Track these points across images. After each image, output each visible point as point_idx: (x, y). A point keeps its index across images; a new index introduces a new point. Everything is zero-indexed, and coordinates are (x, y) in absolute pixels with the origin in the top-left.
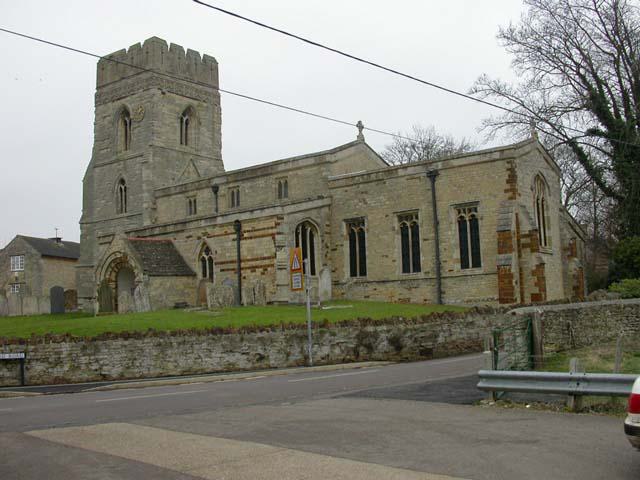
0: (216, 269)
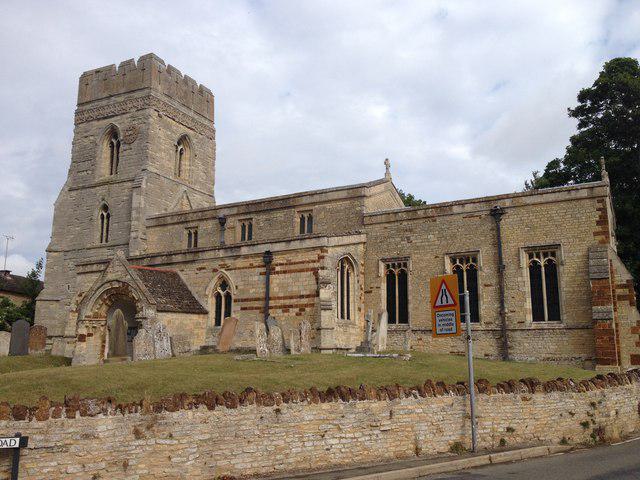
0: (235, 307)
